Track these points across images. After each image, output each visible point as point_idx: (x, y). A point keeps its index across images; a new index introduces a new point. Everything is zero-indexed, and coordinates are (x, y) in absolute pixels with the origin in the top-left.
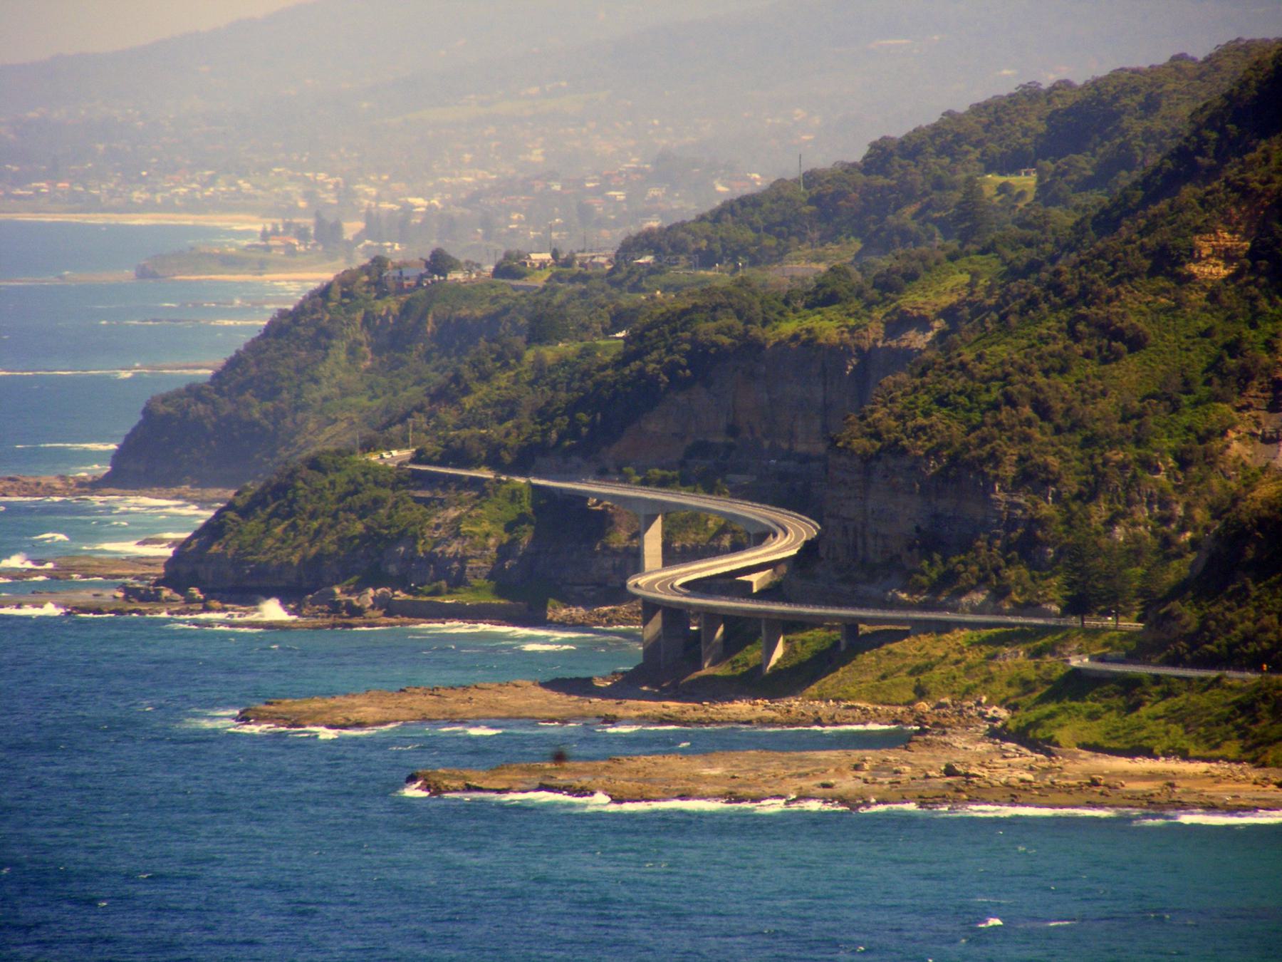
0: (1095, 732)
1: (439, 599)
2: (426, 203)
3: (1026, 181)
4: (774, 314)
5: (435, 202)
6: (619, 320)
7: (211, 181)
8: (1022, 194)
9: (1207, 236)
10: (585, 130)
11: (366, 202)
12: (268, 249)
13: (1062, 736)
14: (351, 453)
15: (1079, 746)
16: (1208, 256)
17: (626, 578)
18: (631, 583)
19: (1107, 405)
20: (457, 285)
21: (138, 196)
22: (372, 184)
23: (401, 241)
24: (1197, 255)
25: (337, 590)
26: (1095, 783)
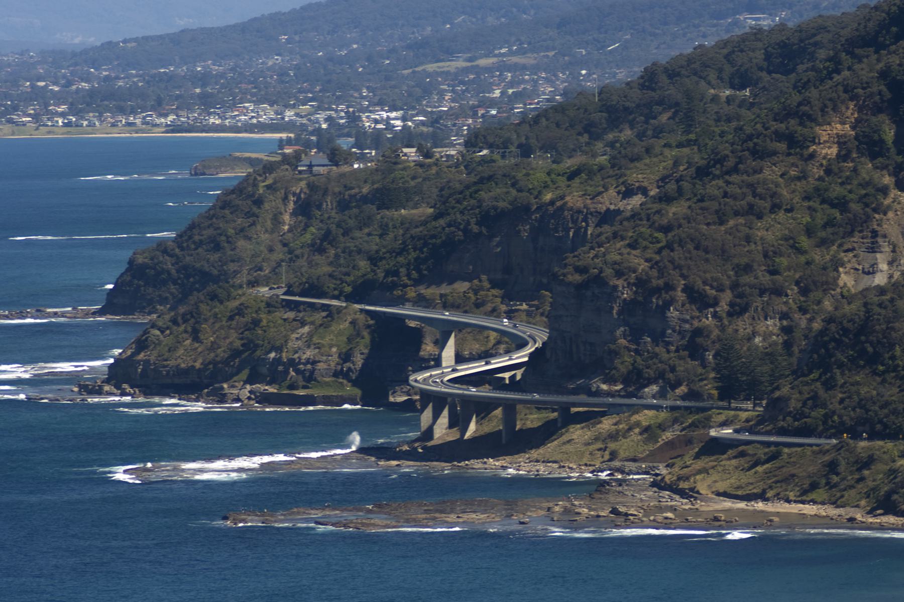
1: (296, 392)
2: (402, 124)
9: (825, 127)
13: (703, 489)
16: (825, 142)
23: (376, 149)
24: (817, 141)
25: (225, 386)
26: (716, 519)
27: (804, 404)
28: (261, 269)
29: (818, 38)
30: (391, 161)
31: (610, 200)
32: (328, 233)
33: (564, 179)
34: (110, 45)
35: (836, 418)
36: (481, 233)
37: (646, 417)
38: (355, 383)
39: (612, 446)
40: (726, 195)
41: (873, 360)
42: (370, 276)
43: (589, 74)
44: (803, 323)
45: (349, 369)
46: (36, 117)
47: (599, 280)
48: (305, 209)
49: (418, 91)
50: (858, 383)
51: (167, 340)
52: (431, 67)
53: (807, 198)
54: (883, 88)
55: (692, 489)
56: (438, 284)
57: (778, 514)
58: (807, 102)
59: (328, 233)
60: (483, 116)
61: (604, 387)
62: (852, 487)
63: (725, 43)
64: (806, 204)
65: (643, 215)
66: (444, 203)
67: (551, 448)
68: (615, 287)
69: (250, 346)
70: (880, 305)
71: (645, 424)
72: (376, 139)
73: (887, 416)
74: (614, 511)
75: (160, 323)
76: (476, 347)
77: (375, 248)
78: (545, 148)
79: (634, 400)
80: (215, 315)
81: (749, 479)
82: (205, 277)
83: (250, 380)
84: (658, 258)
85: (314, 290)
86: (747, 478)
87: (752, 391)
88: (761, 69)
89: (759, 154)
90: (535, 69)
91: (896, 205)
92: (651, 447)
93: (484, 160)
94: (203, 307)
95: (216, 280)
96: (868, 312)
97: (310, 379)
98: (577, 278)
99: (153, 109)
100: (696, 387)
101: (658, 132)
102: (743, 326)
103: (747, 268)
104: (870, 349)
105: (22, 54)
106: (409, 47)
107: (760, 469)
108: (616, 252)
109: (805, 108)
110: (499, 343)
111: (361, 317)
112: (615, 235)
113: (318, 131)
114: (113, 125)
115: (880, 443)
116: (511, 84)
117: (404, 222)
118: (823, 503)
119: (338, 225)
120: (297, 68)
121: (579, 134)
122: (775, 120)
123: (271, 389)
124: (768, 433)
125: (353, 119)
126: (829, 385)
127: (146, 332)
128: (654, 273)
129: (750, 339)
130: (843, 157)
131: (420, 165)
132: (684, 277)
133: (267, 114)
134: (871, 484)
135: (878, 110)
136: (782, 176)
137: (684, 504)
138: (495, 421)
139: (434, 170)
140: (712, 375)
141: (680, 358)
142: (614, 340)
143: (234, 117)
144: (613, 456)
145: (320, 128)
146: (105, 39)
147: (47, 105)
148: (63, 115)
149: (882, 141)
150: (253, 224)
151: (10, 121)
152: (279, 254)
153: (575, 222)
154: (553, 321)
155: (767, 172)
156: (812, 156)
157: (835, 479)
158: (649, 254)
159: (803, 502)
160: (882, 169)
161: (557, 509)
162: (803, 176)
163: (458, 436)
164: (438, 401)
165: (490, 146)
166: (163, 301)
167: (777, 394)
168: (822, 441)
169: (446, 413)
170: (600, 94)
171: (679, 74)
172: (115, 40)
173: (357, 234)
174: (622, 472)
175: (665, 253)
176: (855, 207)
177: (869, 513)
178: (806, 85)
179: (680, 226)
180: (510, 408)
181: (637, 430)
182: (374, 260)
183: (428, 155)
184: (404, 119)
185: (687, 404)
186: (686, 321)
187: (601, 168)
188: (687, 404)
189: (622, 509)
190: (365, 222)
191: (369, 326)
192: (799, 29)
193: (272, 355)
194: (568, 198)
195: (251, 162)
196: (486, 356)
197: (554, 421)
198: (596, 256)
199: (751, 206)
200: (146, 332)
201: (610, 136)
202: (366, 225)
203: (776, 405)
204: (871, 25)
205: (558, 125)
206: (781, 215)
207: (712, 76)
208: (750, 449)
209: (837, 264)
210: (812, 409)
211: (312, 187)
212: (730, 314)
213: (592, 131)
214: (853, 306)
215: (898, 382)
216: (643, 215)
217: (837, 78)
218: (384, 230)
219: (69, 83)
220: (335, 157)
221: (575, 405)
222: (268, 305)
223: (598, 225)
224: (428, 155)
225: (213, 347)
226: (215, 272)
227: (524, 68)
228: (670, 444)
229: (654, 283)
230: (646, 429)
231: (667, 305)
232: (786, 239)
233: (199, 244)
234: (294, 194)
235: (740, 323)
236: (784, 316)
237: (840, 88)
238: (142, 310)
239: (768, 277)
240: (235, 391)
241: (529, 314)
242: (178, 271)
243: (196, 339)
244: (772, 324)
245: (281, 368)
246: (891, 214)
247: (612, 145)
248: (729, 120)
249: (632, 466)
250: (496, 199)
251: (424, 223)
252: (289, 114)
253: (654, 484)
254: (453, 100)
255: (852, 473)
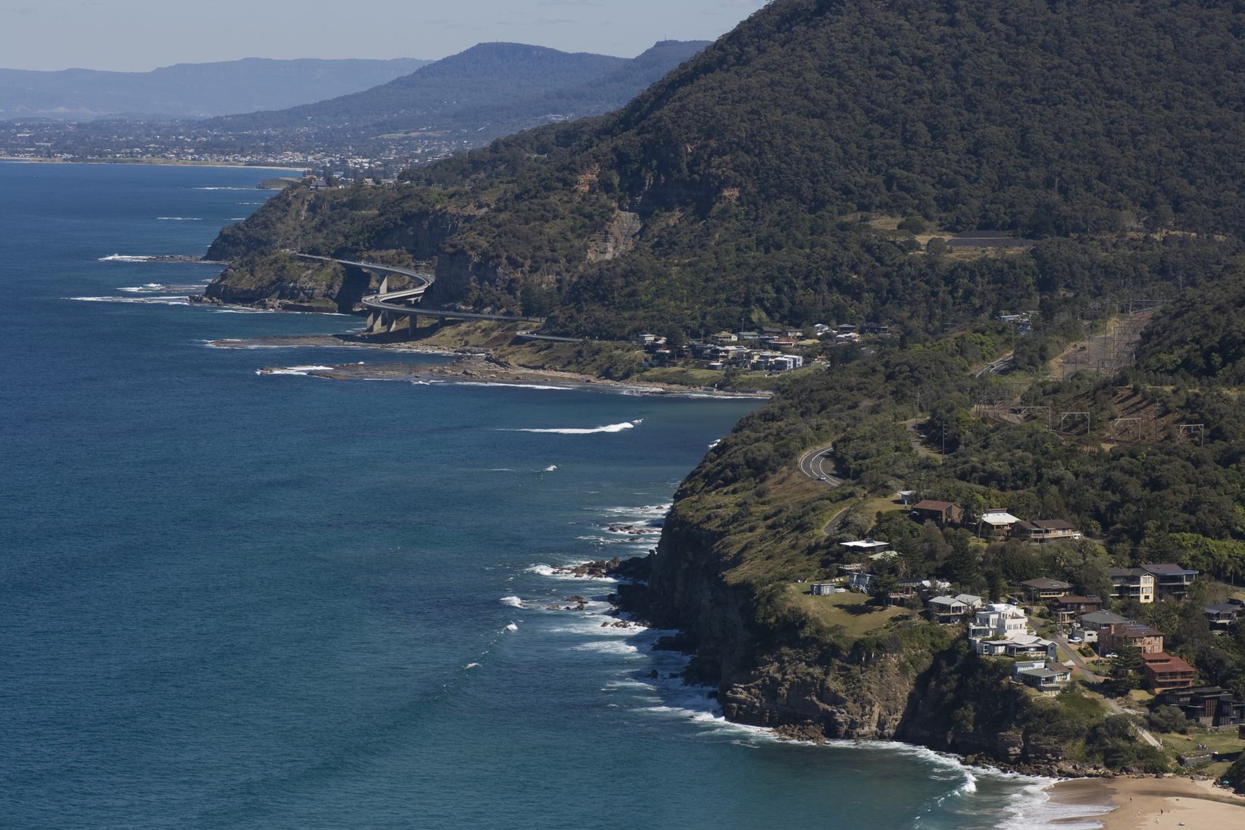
26: (518, 378)
27: (566, 321)
28: (288, 239)
29: (583, 129)
30: (359, 185)
31: (471, 210)
32: (324, 222)
33: (447, 198)
34: (218, 118)
35: (582, 328)
36: (402, 225)
37: (484, 324)
38: (335, 300)
39: (466, 338)
40: (530, 209)
41: (603, 298)
42: (344, 245)
43: (468, 143)
44: (568, 278)
45: (331, 293)
46: (177, 155)
47: (462, 252)
48: (313, 208)
49: (378, 148)
50: (594, 310)
51: (238, 275)
52: (386, 136)
53: (572, 213)
54: (614, 157)
55: (506, 363)
56: (380, 249)
57: (550, 377)
58: (573, 162)
59: (324, 222)
60: (411, 163)
61: (463, 307)
62: (589, 364)
63: (535, 130)
64: (571, 215)
65: (486, 219)
66: (384, 208)
67: (434, 338)
68: (470, 256)
69: (281, 279)
70: (607, 270)
71: (483, 327)
72: (355, 173)
73: (609, 328)
74: (465, 373)
75: (234, 266)
76: (398, 284)
77: (347, 230)
78: (439, 182)
79: (478, 315)
80: (263, 263)
81: (536, 358)
82: (260, 242)
83: (279, 298)
84: (493, 241)
85: (314, 251)
86: (535, 357)
87: (540, 313)
88: (553, 144)
89: (548, 189)
90: (440, 139)
91: (618, 218)
92: (486, 340)
93: (407, 187)
94: (256, 258)
95: (265, 244)
96: (601, 273)
97: (311, 297)
98: (451, 250)
99: (239, 153)
100: (511, 309)
101: (498, 175)
102: (536, 278)
103: (540, 248)
104: (601, 293)
105: (172, 121)
106: (375, 125)
107: (542, 353)
108: (472, 237)
109: (573, 166)
110: (410, 282)
111: (339, 267)
112: (471, 228)
113: (324, 168)
114: (218, 161)
115: (605, 342)
116: (427, 147)
117: (364, 218)
118: (574, 372)
119: (329, 218)
120: (316, 134)
121: (458, 175)
122: (557, 171)
123: (291, 302)
124: (546, 335)
125: (343, 162)
126: (579, 311)
127: (226, 270)
128: (491, 249)
129: (540, 285)
130: (592, 191)
131: (374, 188)
132: (507, 252)
133: (299, 158)
134: (599, 363)
135: (611, 168)
136: (559, 200)
137: (501, 370)
138: (405, 323)
139: (381, 191)
140: (519, 303)
141: (503, 294)
142: (469, 283)
143: (281, 159)
144: (466, 343)
145: (326, 166)
146: (215, 116)
147: (183, 149)
148: (191, 154)
149: (612, 184)
150: (286, 215)
151: (164, 156)
152: (299, 232)
153: (452, 220)
154: (438, 273)
155: (551, 199)
156: (575, 191)
157: (581, 359)
158: (489, 239)
159: (563, 371)
160: (612, 198)
161: (435, 370)
162: (570, 201)
163: (386, 330)
164: (376, 312)
165: (411, 179)
166: (237, 254)
167: (552, 314)
168: (574, 340)
169: (380, 318)
170: (469, 153)
171: (510, 145)
172: (221, 115)
173: (339, 222)
174: (471, 352)
175: (497, 238)
176: (597, 218)
177: (598, 378)
178: (574, 154)
179: (505, 225)
180: (414, 317)
181: (479, 331)
182: (346, 237)
183: (378, 183)
184: (370, 163)
185: (506, 318)
186: (506, 274)
187: (467, 193)
188: (506, 318)
189: (469, 372)
190: (344, 217)
191: (342, 271)
192: (574, 124)
193: (292, 285)
194: (448, 208)
195: (287, 182)
196: (403, 288)
197: (437, 324)
198: (461, 239)
199: (543, 216)
200: (226, 270)
201: (474, 176)
202: (344, 218)
203: (551, 321)
204: (610, 123)
205: (446, 169)
206: (558, 221)
207: (528, 147)
208: (537, 343)
209: (586, 247)
210: (570, 322)
211: (317, 197)
212: (529, 272)
213: (464, 173)
214: (594, 270)
215: (615, 311)
216: (486, 219)
217: (590, 150)
218: (353, 221)
219: (196, 138)
220: (330, 182)
221: (447, 316)
222: (290, 258)
223: (464, 223)
224: (378, 183)
225: (261, 279)
226: (265, 240)
227: (434, 138)
228: (496, 338)
229: (491, 254)
230: (484, 330)
231: (497, 266)
232: (561, 233)
233: (257, 225)
234: (308, 201)
235: (535, 277)
236: (558, 274)
237: (591, 156)
238: (226, 258)
239: (550, 253)
240: (271, 303)
241: (426, 268)
242: (246, 239)
243: (252, 275)
244: (552, 278)
245: (296, 291)
246: (615, 223)
247: (474, 181)
248: (534, 170)
249: (476, 349)
250: (411, 207)
251: (374, 218)
252: (310, 158)
253: (486, 359)
254: (396, 154)
255: (589, 357)
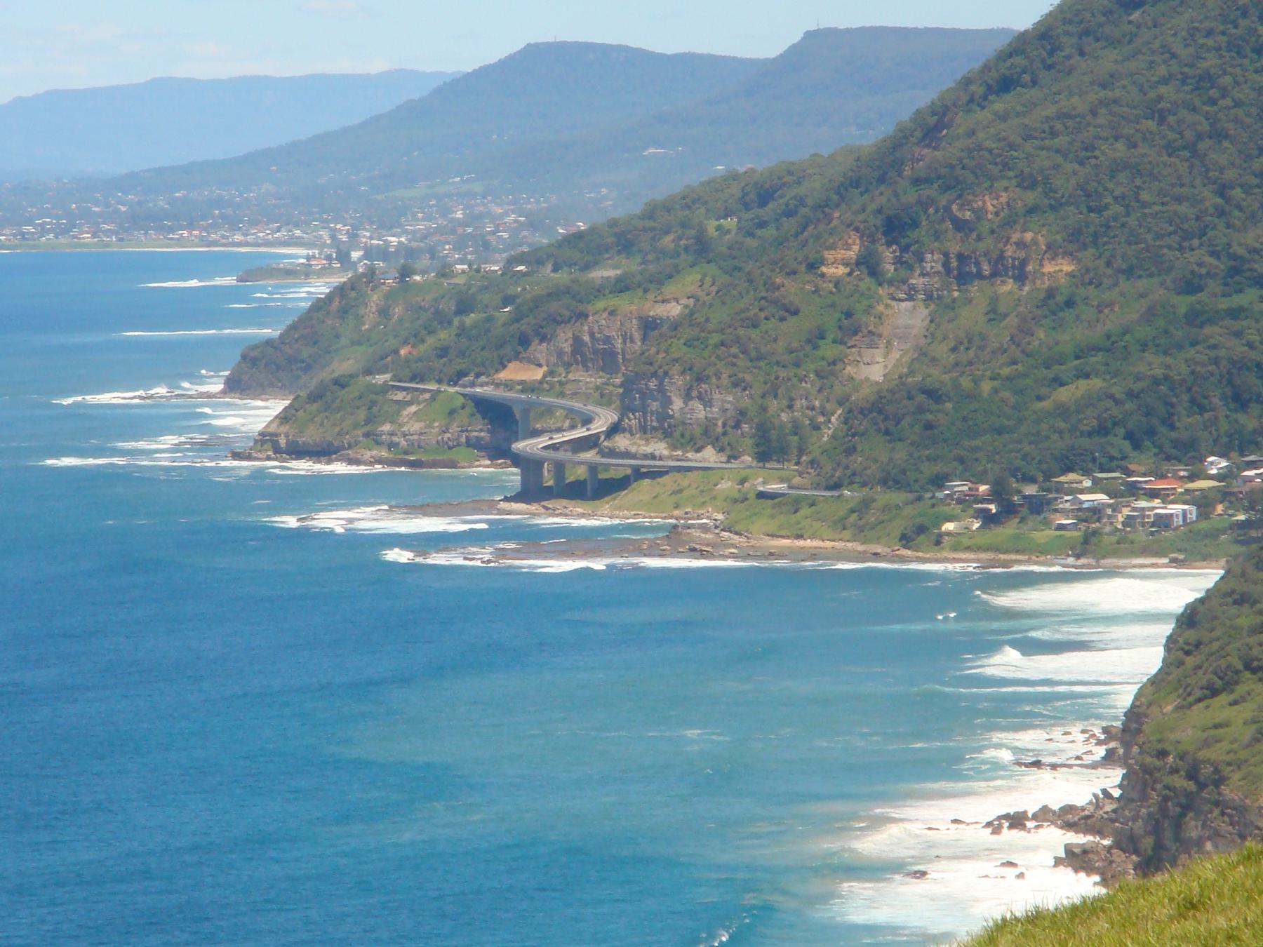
0: (772, 526)
3: (731, 223)
4: (592, 297)
5: (403, 239)
6: (507, 300)
7: (279, 230)
8: (729, 231)
10: (486, 201)
11: (364, 240)
12: (311, 266)
14: (357, 376)
15: (764, 535)
17: (511, 444)
18: (513, 446)
19: (780, 346)
20: (416, 283)
21: (238, 237)
22: (367, 230)
